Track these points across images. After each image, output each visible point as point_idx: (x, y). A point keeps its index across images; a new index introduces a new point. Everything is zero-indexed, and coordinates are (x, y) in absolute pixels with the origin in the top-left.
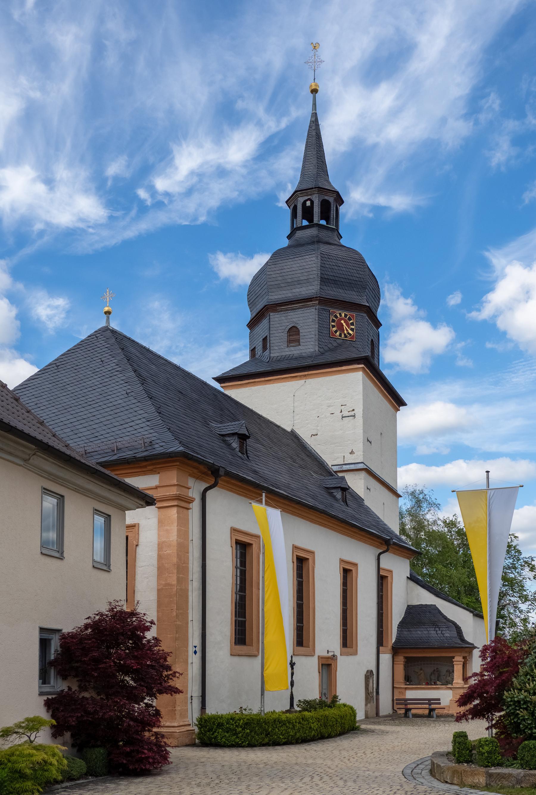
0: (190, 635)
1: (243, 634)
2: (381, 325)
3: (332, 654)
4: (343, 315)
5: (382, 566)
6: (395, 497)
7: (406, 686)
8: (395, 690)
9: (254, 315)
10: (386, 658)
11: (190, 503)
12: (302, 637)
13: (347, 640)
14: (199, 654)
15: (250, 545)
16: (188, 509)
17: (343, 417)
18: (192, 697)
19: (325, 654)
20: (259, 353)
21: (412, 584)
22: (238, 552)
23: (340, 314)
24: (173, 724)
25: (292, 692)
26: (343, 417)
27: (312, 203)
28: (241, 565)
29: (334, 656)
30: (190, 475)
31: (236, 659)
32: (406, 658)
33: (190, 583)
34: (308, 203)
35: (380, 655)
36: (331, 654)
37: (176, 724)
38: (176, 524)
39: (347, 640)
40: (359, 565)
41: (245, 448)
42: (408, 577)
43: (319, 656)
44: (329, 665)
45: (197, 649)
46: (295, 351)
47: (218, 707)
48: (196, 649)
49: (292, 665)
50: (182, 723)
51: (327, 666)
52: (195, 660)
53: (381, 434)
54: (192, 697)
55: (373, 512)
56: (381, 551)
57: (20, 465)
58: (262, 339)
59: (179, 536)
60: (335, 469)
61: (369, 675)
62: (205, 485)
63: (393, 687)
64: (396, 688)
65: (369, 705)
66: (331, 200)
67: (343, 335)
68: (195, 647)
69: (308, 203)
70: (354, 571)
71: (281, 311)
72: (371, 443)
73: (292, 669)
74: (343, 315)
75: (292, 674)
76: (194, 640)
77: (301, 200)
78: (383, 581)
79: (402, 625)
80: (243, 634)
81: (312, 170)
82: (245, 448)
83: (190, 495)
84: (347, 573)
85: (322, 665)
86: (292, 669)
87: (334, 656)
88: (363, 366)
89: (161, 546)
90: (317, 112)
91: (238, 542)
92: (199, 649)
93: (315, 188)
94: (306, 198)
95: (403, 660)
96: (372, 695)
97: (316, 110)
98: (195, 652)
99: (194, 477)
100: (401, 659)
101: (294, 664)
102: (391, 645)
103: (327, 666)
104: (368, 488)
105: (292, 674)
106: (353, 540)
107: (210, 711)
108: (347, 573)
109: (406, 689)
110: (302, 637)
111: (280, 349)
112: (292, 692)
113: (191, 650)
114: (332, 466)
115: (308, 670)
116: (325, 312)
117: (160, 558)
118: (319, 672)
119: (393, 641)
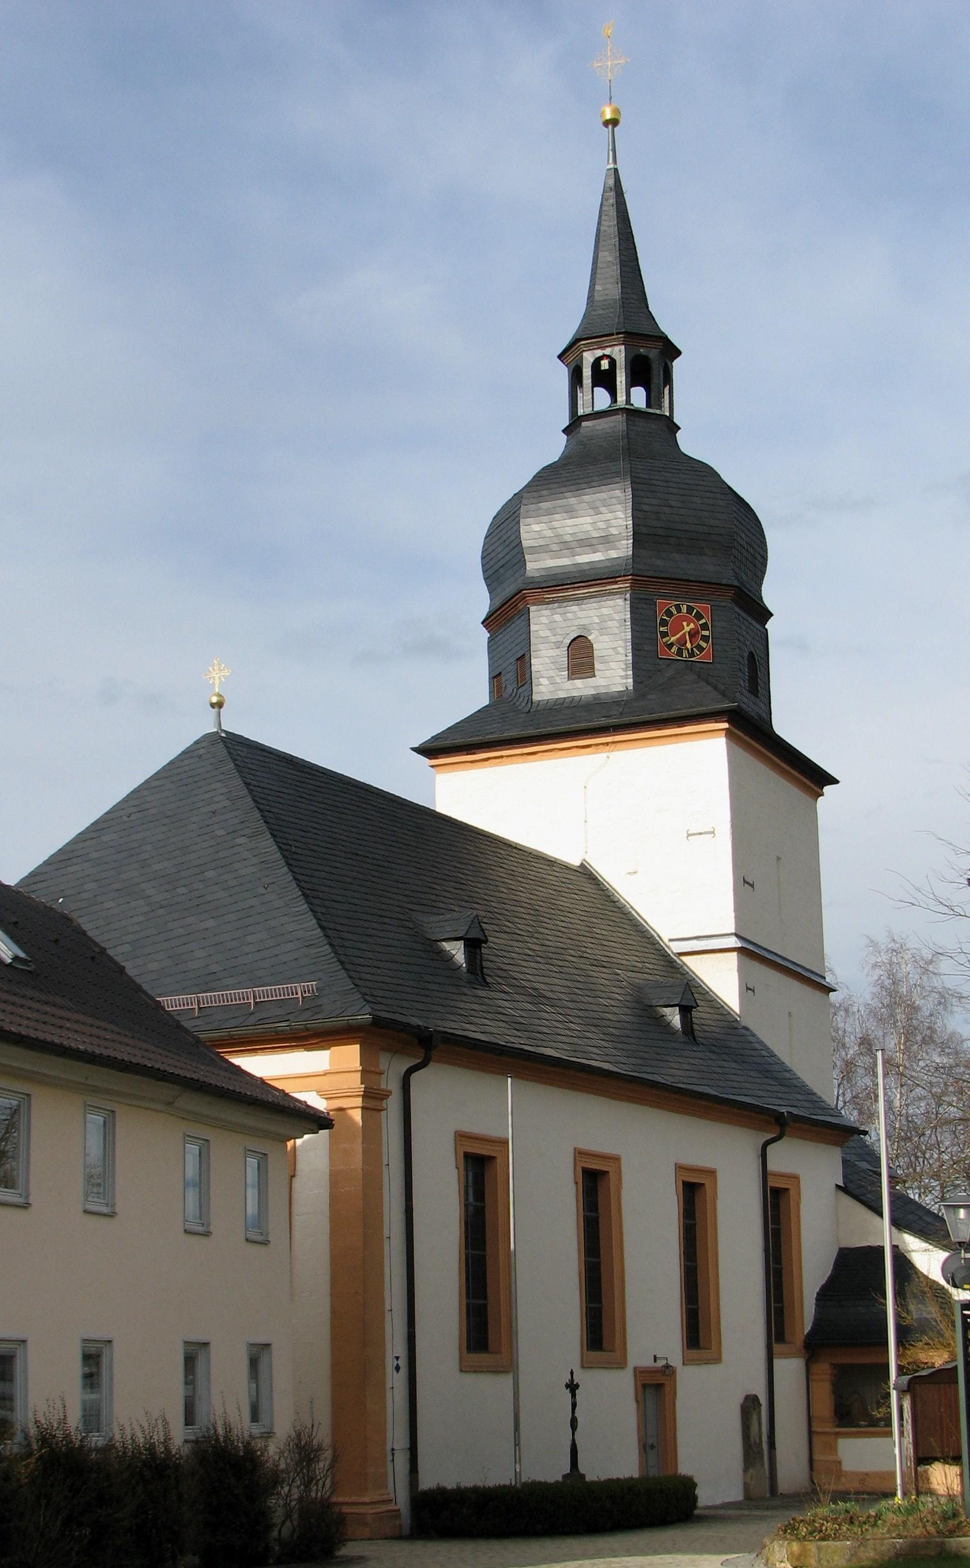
0: (388, 1337)
1: (484, 1329)
2: (772, 615)
3: (664, 1362)
4: (684, 609)
5: (771, 1167)
6: (818, 994)
7: (837, 1430)
8: (815, 1439)
9: (498, 603)
10: (790, 1370)
11: (382, 1099)
12: (600, 1330)
13: (698, 1330)
14: (404, 1371)
15: (492, 1159)
16: (380, 1110)
17: (689, 835)
18: (393, 1450)
19: (648, 1363)
20: (510, 689)
21: (846, 1201)
22: (470, 1174)
23: (679, 610)
24: (363, 1499)
25: (574, 1440)
26: (689, 835)
27: (613, 363)
28: (476, 1200)
29: (667, 1366)
30: (383, 1049)
31: (470, 1378)
32: (834, 1366)
33: (386, 1242)
34: (605, 365)
35: (776, 1362)
36: (661, 1363)
37: (367, 1499)
38: (360, 1140)
39: (698, 1330)
40: (719, 1175)
41: (478, 962)
42: (837, 1186)
43: (635, 1369)
44: (659, 1387)
45: (400, 1362)
46: (582, 688)
47: (437, 1474)
48: (400, 1362)
49: (572, 1387)
50: (376, 1498)
51: (655, 1387)
52: (397, 1382)
53: (778, 859)
54: (393, 1450)
55: (761, 1043)
56: (770, 1136)
57: (161, 1112)
58: (512, 660)
59: (365, 1161)
60: (677, 947)
61: (750, 1405)
62: (404, 1064)
63: (811, 1433)
64: (817, 1433)
65: (751, 1471)
66: (653, 354)
67: (685, 653)
68: (397, 1358)
69: (605, 365)
70: (707, 1187)
71: (553, 602)
72: (752, 886)
73: (574, 1395)
74: (684, 609)
75: (574, 1405)
76: (395, 1346)
77: (589, 358)
78: (777, 1202)
79: (826, 1294)
80: (484, 1329)
81: (611, 289)
82: (478, 962)
83: (383, 1086)
84: (694, 1193)
85: (644, 1386)
86: (574, 1395)
87: (667, 1366)
88: (726, 725)
89: (336, 1179)
90: (619, 166)
91: (467, 1156)
92: (403, 1363)
93: (618, 334)
94: (599, 353)
95: (829, 1372)
96: (757, 1449)
97: (615, 162)
98: (398, 1368)
99: (388, 1050)
100: (823, 1369)
101: (577, 1386)
102: (803, 1338)
103: (655, 1387)
104: (748, 989)
105: (574, 1405)
106: (703, 1121)
107: (427, 1482)
108: (694, 1193)
109: (837, 1434)
110: (600, 1330)
111: (550, 681)
112: (574, 1440)
113: (390, 1364)
114: (671, 940)
115: (612, 1396)
116: (644, 606)
117: (334, 1199)
118: (637, 1401)
119: (808, 1328)
